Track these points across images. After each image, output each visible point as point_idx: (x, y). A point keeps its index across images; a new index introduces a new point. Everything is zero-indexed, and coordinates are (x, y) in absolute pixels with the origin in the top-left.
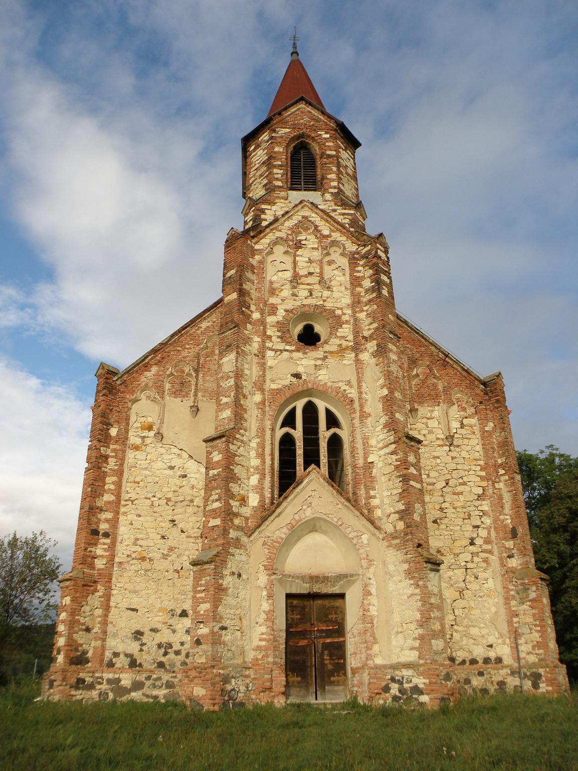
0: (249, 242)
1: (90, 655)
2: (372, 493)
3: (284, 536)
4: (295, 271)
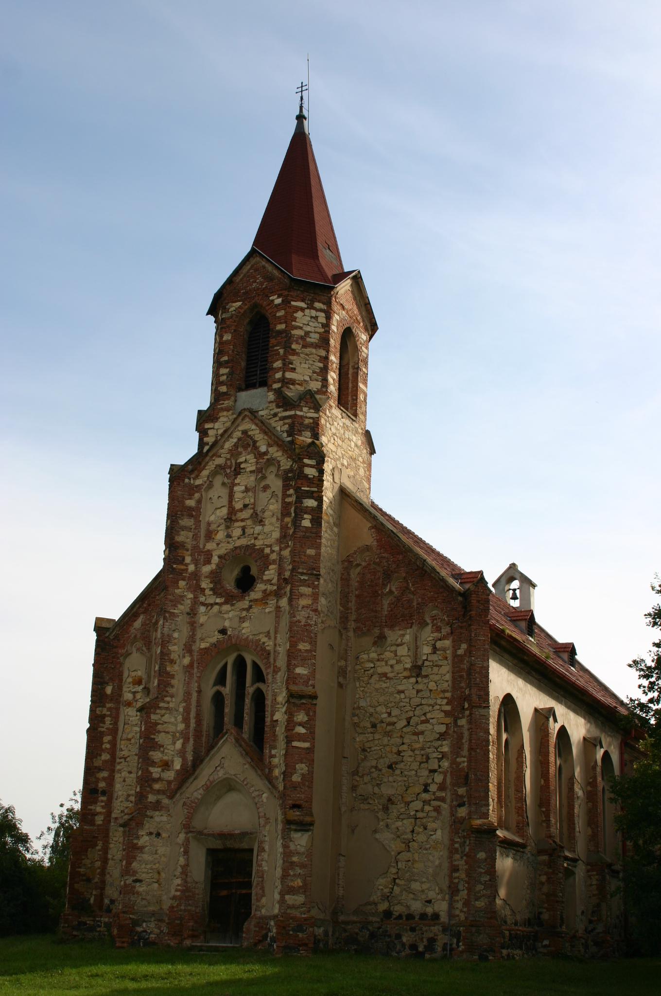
2: (273, 752)
3: (200, 797)
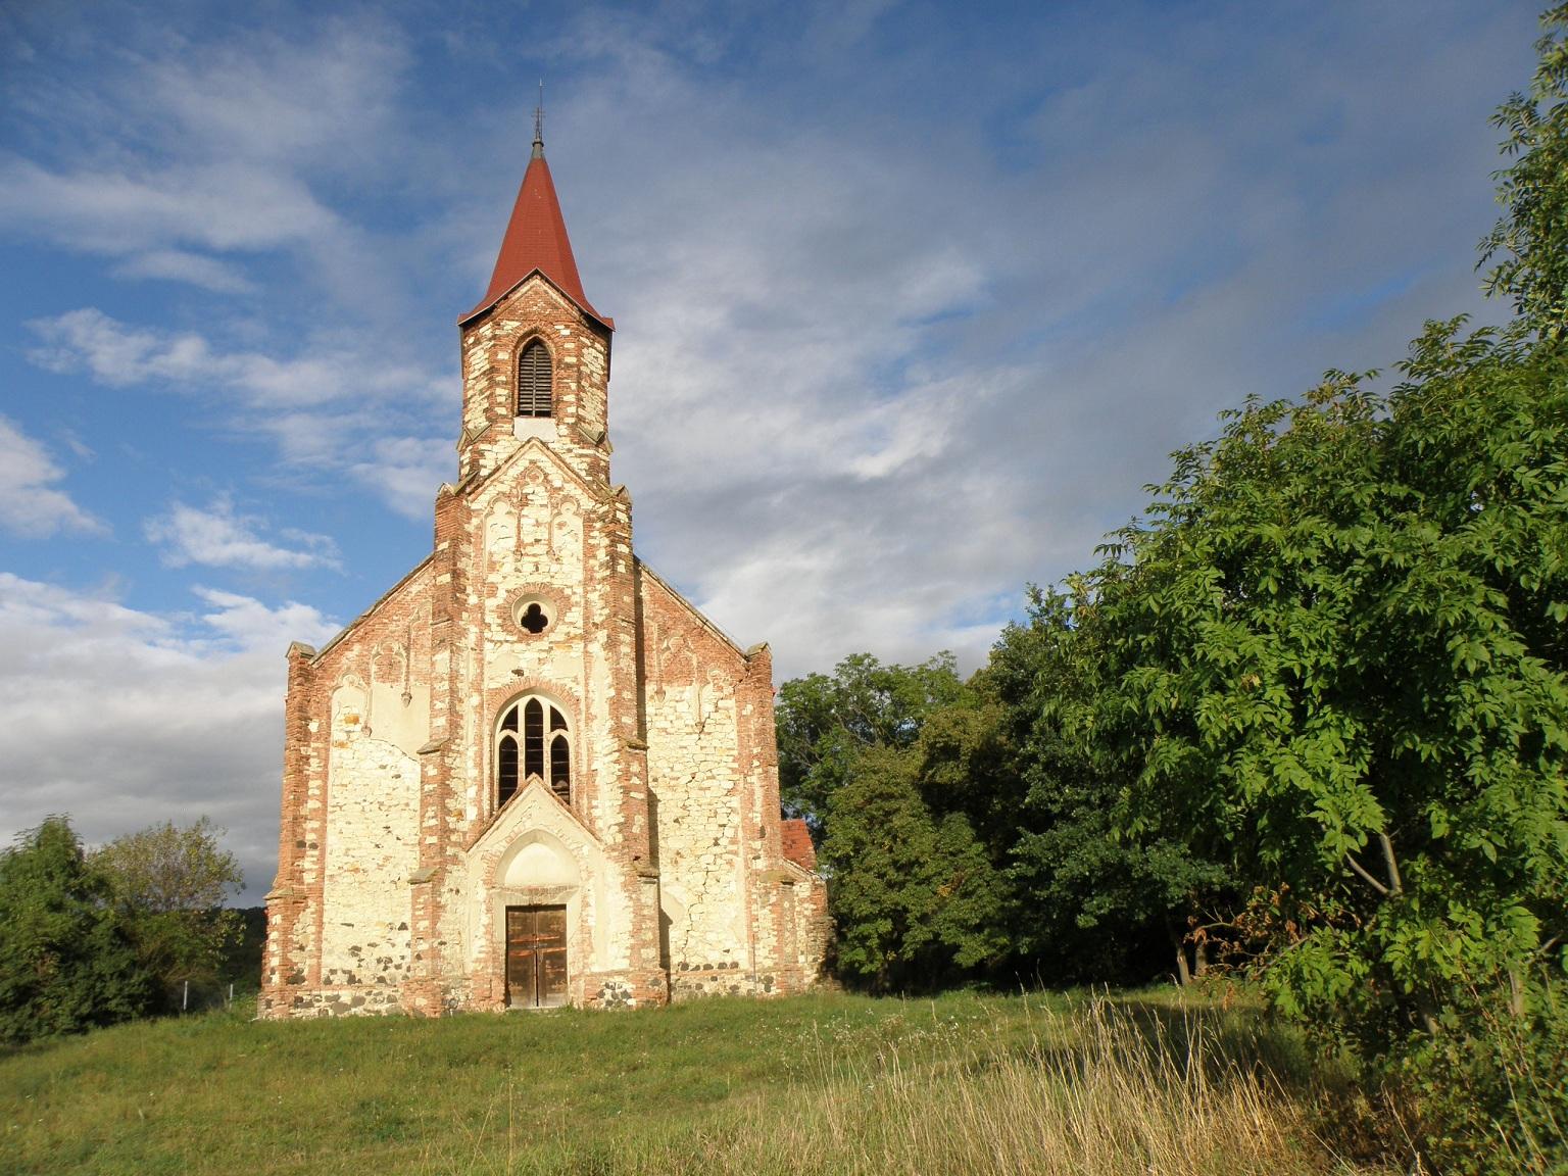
0: (465, 503)
1: (305, 973)
2: (594, 803)
4: (519, 538)
